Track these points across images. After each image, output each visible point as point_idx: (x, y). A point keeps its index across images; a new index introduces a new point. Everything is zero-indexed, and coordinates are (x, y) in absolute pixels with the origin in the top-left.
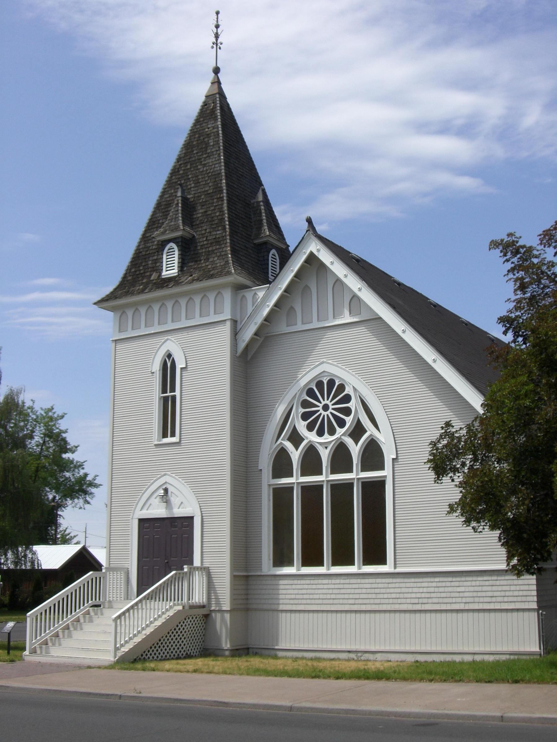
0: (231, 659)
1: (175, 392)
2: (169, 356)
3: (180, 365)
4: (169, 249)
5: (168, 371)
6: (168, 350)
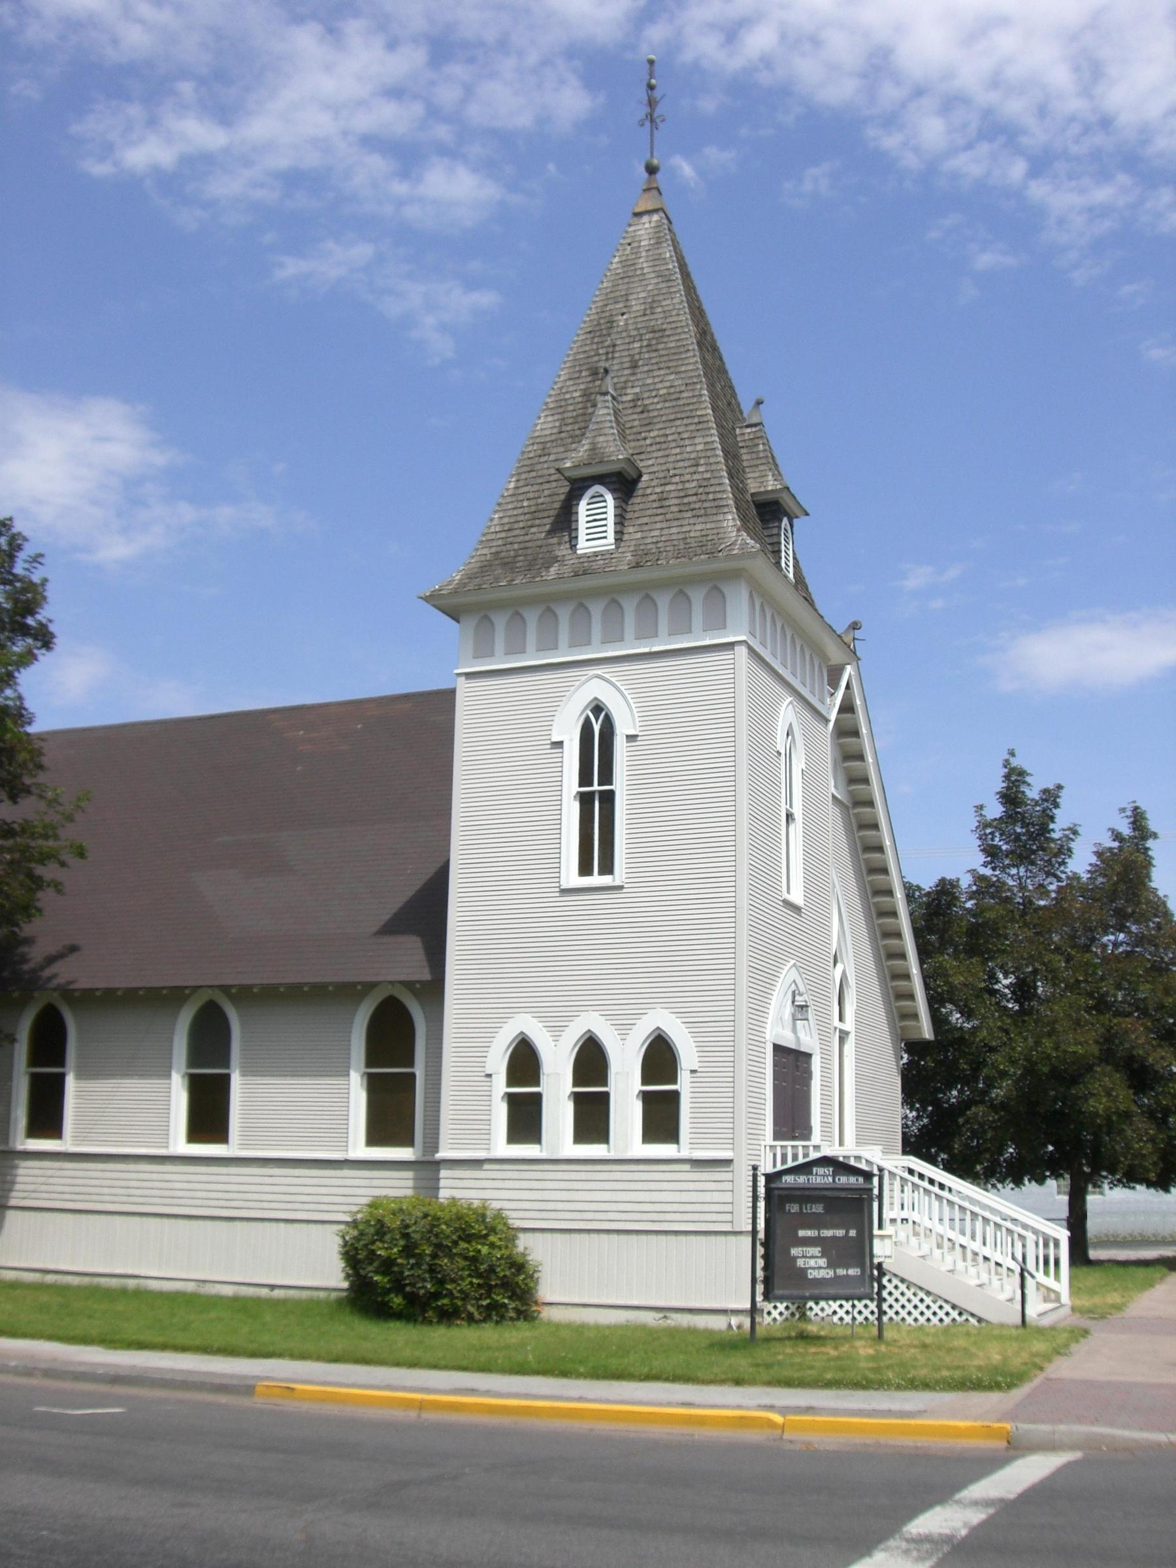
0: (746, 1377)
1: (537, 1084)
2: (598, 708)
3: (622, 729)
4: (593, 497)
5: (598, 745)
6: (596, 699)
